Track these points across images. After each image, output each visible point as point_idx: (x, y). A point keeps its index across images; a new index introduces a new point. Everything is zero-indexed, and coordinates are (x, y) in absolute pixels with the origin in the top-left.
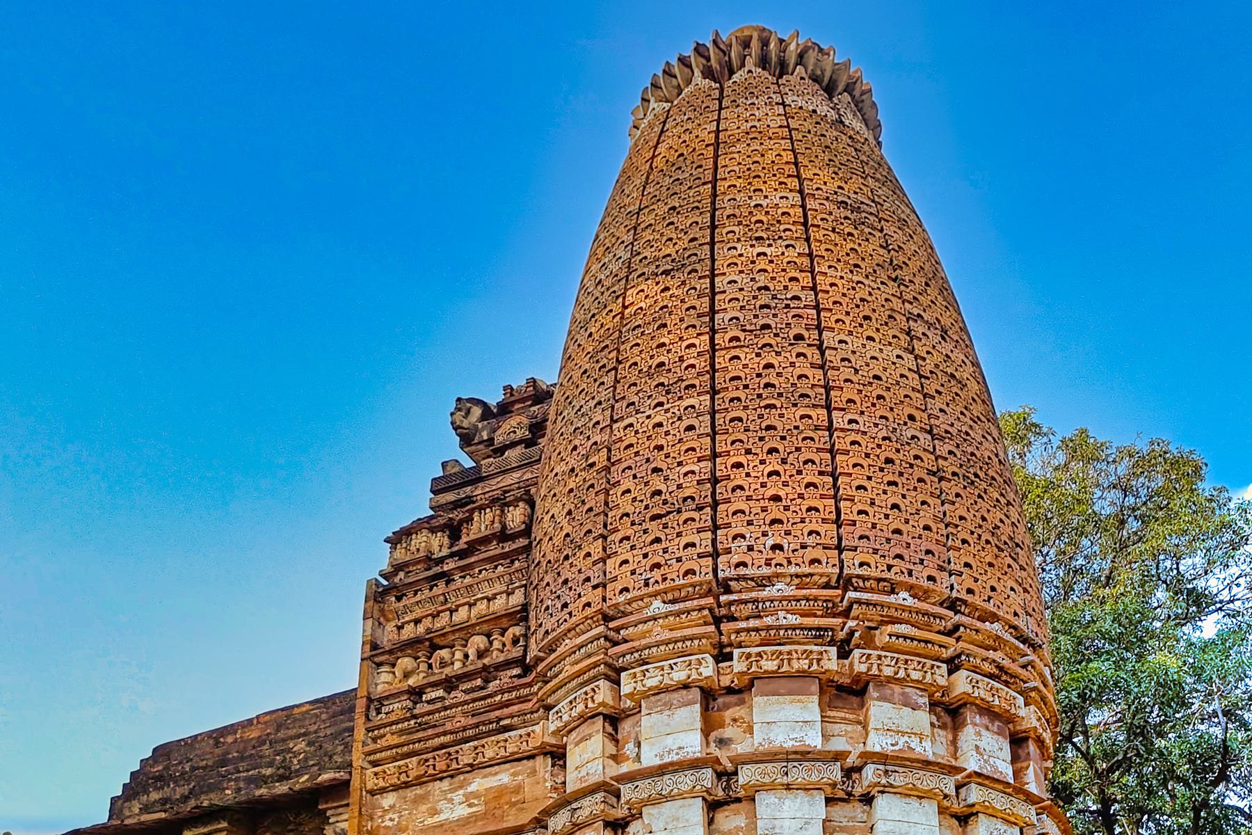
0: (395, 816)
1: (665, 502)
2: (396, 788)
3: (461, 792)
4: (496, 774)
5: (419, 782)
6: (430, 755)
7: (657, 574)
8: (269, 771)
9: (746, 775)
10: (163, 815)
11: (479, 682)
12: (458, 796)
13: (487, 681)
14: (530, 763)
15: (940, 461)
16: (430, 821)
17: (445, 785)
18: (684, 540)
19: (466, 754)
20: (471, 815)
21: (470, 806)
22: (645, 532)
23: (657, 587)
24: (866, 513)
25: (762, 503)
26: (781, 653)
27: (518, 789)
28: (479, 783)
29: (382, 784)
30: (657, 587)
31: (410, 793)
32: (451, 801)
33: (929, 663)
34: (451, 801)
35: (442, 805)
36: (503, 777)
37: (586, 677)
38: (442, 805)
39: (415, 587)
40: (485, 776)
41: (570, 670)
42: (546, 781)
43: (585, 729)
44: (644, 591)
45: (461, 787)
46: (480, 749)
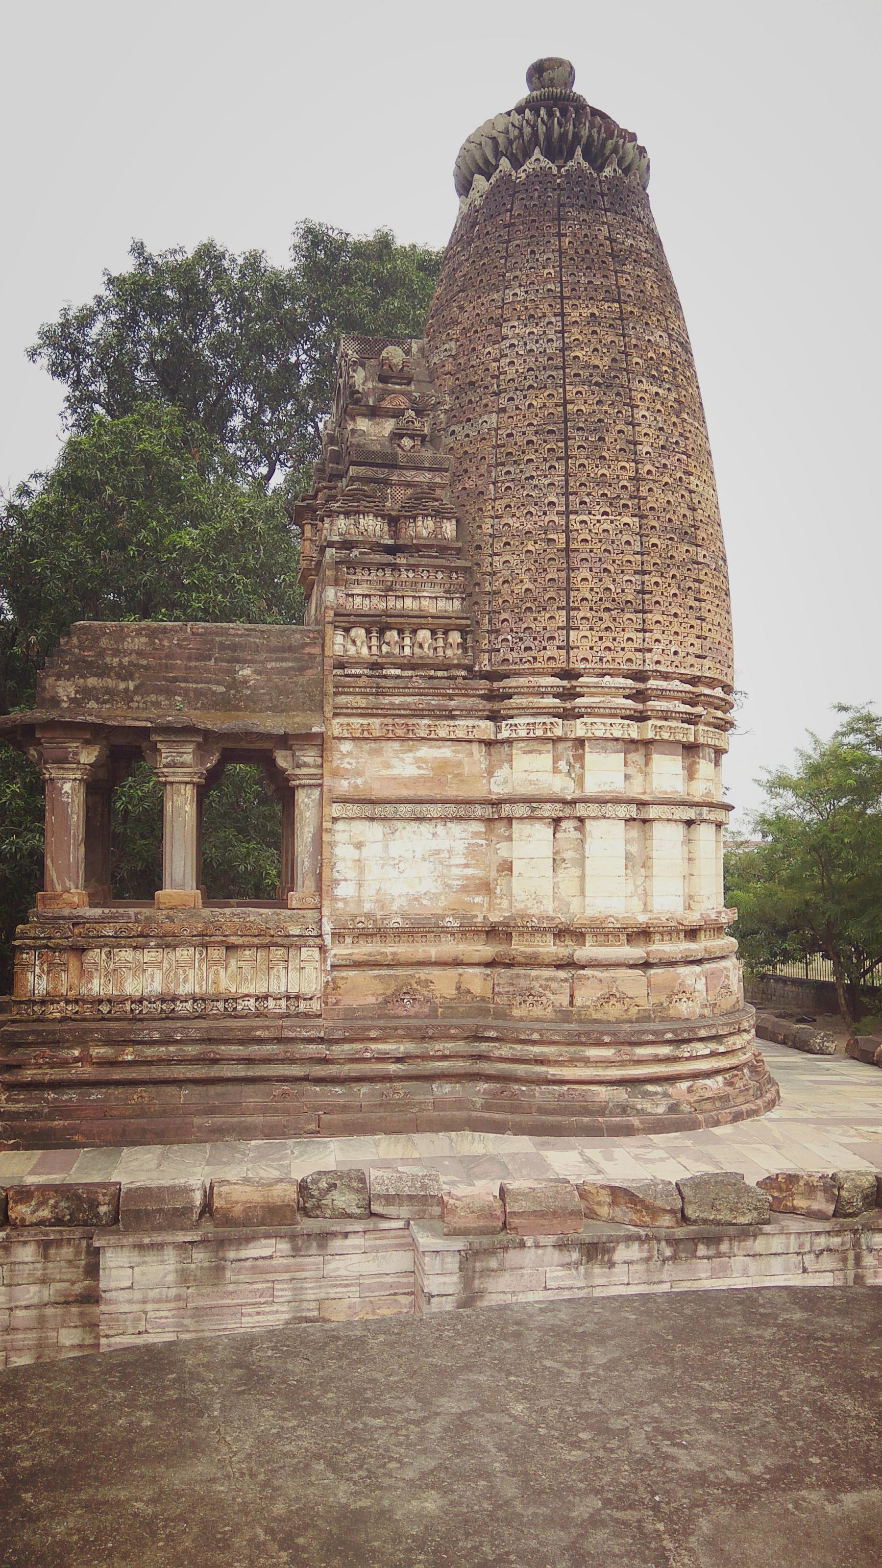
2: (354, 739)
3: (411, 755)
4: (440, 747)
7: (608, 656)
12: (409, 757)
14: (467, 746)
15: (283, 964)
16: (384, 772)
17: (396, 745)
18: (627, 635)
20: (421, 777)
21: (419, 767)
22: (601, 619)
27: (460, 764)
28: (425, 751)
31: (366, 746)
32: (402, 760)
33: (366, 735)
34: (402, 760)
35: (394, 761)
36: (446, 752)
38: (394, 761)
40: (430, 747)
42: (481, 763)
45: (411, 751)
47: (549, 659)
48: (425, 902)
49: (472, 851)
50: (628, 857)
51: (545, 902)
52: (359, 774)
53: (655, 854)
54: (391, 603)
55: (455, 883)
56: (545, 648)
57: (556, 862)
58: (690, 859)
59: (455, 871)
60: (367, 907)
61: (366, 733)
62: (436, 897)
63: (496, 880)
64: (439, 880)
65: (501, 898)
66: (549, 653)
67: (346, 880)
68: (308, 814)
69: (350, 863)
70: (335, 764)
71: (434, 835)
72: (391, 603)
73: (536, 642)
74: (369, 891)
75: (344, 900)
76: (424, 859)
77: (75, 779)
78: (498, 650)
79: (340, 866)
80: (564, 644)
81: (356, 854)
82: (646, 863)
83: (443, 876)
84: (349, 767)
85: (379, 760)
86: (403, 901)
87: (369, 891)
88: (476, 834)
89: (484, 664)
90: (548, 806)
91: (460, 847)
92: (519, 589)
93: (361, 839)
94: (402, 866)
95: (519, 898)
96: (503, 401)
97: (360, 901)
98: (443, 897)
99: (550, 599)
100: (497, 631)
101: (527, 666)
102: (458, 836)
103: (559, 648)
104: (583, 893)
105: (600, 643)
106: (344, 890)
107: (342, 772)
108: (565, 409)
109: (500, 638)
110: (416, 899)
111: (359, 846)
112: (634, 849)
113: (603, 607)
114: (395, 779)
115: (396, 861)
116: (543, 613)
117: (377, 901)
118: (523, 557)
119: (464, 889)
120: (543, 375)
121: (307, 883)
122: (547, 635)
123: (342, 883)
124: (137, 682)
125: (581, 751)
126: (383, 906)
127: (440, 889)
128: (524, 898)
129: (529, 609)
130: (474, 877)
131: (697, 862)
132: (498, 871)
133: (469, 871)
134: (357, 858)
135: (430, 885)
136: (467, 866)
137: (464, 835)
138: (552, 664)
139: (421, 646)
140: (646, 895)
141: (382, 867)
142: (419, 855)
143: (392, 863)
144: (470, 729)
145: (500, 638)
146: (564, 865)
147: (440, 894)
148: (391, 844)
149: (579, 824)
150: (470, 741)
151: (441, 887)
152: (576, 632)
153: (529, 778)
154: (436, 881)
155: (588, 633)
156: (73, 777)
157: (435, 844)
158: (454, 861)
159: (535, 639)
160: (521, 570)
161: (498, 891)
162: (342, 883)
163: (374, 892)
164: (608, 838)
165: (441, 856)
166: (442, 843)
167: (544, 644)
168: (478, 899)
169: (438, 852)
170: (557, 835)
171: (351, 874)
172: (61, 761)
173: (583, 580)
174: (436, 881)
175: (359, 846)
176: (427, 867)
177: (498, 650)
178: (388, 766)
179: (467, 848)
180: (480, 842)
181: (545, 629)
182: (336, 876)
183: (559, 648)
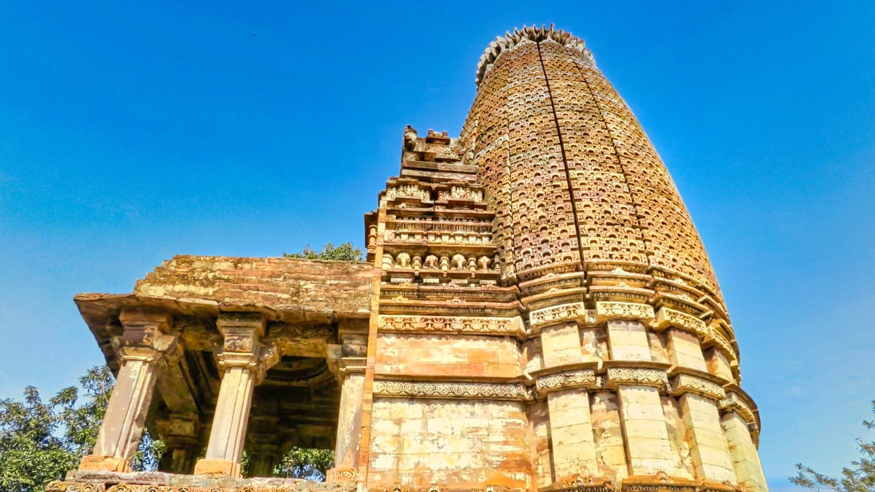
0: (396, 351)
1: (613, 218)
5: (418, 333)
6: (429, 317)
8: (285, 296)
9: (685, 381)
10: (216, 303)
11: (466, 281)
13: (441, 282)
19: (458, 323)
21: (456, 356)
23: (617, 260)
24: (595, 242)
25: (604, 226)
26: (444, 320)
29: (390, 326)
30: (617, 260)
32: (441, 350)
34: (441, 350)
35: (433, 351)
36: (482, 345)
37: (566, 298)
39: (411, 215)
41: (554, 291)
43: (568, 329)
44: (610, 260)
46: (467, 323)
47: (565, 259)
48: (465, 477)
49: (510, 430)
50: (670, 429)
51: (589, 466)
52: (401, 361)
53: (695, 424)
54: (431, 239)
55: (495, 459)
56: (560, 251)
57: (598, 433)
58: (731, 448)
59: (494, 447)
60: (405, 480)
61: (408, 325)
62: (476, 472)
63: (537, 460)
64: (479, 456)
65: (544, 477)
66: (564, 254)
67: (384, 453)
68: (352, 396)
69: (389, 438)
70: (378, 352)
71: (472, 414)
72: (431, 239)
73: (553, 249)
74: (408, 464)
75: (382, 473)
76: (462, 435)
77: (145, 362)
78: (522, 260)
79: (379, 440)
80: (577, 246)
81: (395, 429)
82: (690, 436)
83: (482, 452)
84: (392, 355)
85: (419, 350)
86: (442, 476)
87: (408, 464)
88: (513, 415)
89: (510, 273)
90: (579, 374)
91: (498, 425)
92: (534, 217)
93: (401, 416)
94: (441, 441)
95: (561, 467)
96: (512, 126)
97: (397, 473)
98: (483, 473)
99: (560, 220)
100: (520, 248)
101: (547, 266)
102: (495, 414)
103: (573, 249)
104: (628, 461)
105: (607, 245)
106: (383, 463)
107: (385, 359)
108: (556, 122)
109: (522, 252)
110: (456, 474)
111: (399, 422)
112: (673, 422)
113: (605, 222)
114: (434, 365)
115: (436, 437)
116: (556, 229)
117: (416, 475)
118: (536, 198)
119: (504, 466)
120: (538, 110)
121: (347, 458)
122: (561, 242)
123: (381, 456)
124: (215, 289)
125: (604, 336)
126: (421, 480)
127: (480, 464)
128: (567, 465)
129: (545, 228)
130: (514, 454)
131: (738, 447)
132: (538, 451)
133: (509, 449)
134: (396, 432)
135: (468, 461)
136: (506, 443)
137: (501, 414)
138: (568, 262)
139: (456, 266)
140: (695, 467)
141: (421, 443)
142: (457, 432)
143: (430, 438)
144: (501, 324)
145: (522, 252)
146: (604, 435)
147: (481, 470)
148: (430, 421)
149: (612, 396)
150: (501, 337)
151: (481, 463)
152: (586, 238)
153: (559, 356)
154: (476, 457)
155: (597, 239)
156: (144, 358)
157: (474, 423)
158: (492, 438)
159: (551, 246)
160: (535, 206)
161: (540, 471)
162: (381, 456)
163: (412, 466)
164: (643, 407)
165: (480, 433)
166: (480, 422)
167: (560, 248)
168: (520, 476)
169: (477, 429)
170: (594, 407)
171: (391, 448)
172: (137, 344)
173: (585, 206)
174: (476, 457)
175: (399, 422)
176: (465, 444)
177: (522, 260)
178: (428, 355)
179: (504, 427)
180: (518, 421)
181: (559, 238)
182: (374, 449)
183: (573, 249)
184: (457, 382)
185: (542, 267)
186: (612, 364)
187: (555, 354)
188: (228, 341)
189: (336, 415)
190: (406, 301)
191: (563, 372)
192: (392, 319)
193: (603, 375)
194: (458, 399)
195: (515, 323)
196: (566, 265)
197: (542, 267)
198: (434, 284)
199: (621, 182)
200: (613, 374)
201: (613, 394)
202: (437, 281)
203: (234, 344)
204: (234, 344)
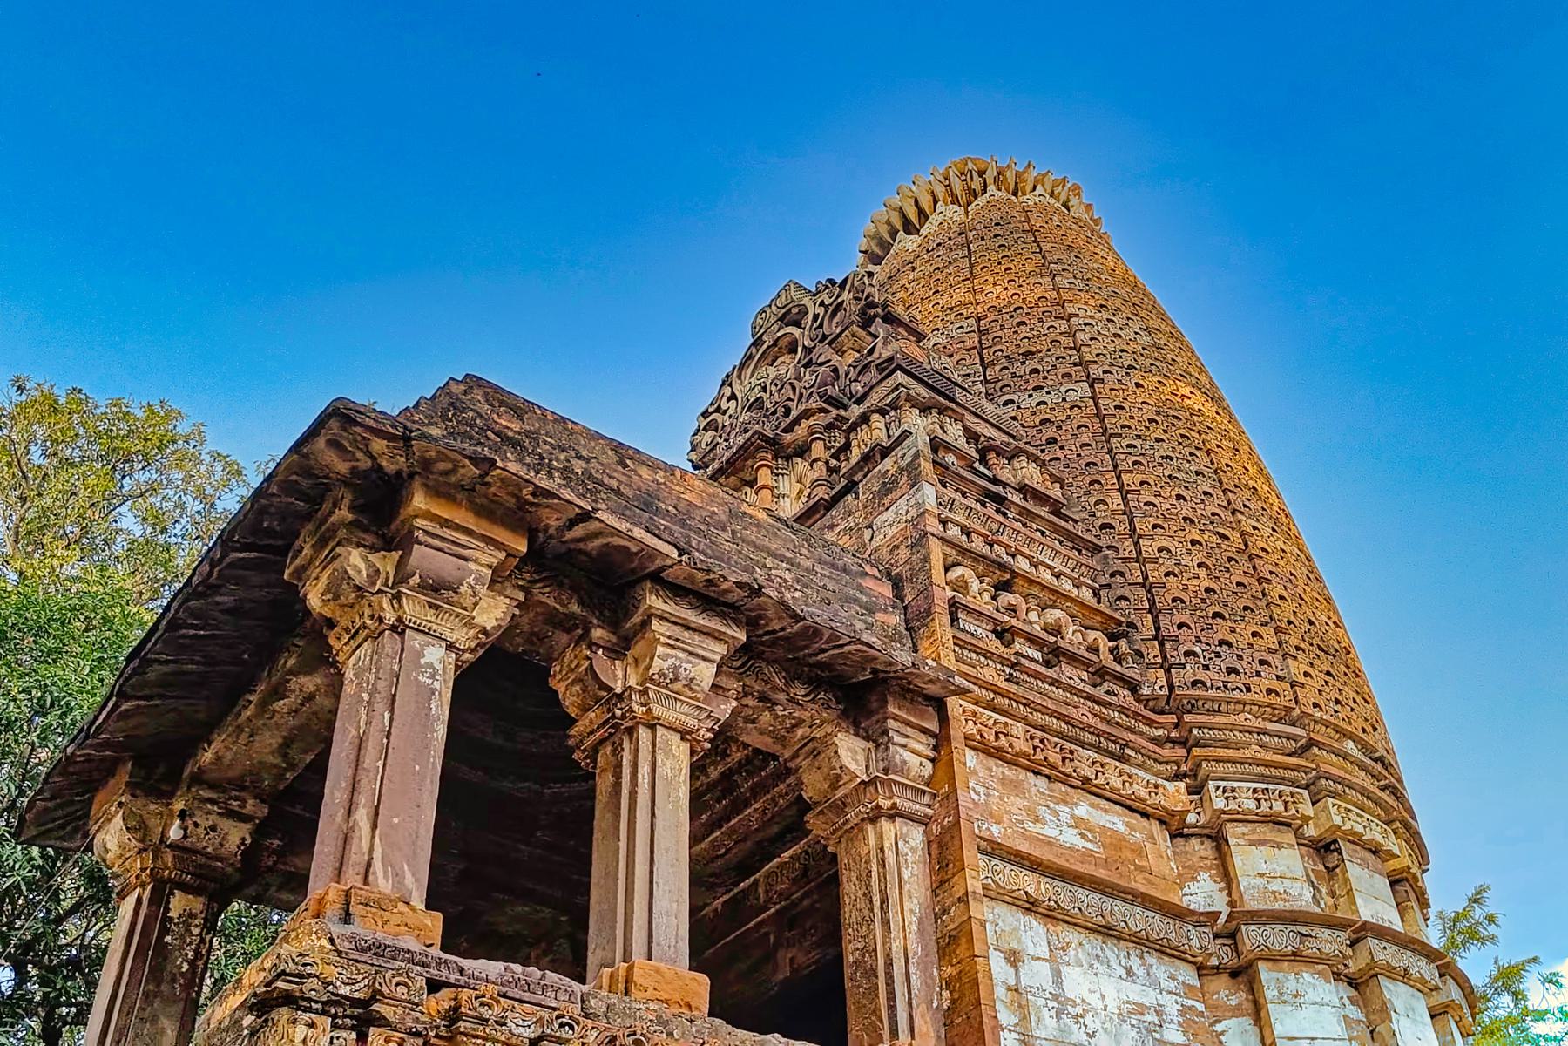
6: (1039, 734)
21: (1083, 836)
138: (1273, 699)
184: (1109, 895)
185: (1227, 694)
186: (1241, 917)
187: (1259, 881)
188: (664, 658)
189: (586, 889)
190: (1254, 723)
191: (1294, 922)
192: (975, 714)
193: (1231, 936)
194: (1106, 931)
195: (1175, 794)
196: (1269, 705)
197: (1227, 694)
198: (1033, 660)
199: (1114, 513)
200: (1251, 936)
201: (1243, 973)
202: (1037, 655)
203: (676, 668)
204: (676, 668)
